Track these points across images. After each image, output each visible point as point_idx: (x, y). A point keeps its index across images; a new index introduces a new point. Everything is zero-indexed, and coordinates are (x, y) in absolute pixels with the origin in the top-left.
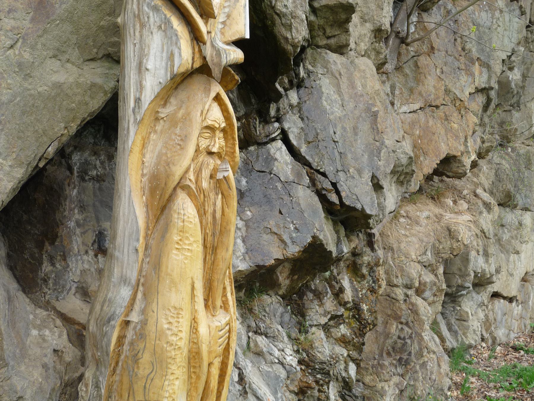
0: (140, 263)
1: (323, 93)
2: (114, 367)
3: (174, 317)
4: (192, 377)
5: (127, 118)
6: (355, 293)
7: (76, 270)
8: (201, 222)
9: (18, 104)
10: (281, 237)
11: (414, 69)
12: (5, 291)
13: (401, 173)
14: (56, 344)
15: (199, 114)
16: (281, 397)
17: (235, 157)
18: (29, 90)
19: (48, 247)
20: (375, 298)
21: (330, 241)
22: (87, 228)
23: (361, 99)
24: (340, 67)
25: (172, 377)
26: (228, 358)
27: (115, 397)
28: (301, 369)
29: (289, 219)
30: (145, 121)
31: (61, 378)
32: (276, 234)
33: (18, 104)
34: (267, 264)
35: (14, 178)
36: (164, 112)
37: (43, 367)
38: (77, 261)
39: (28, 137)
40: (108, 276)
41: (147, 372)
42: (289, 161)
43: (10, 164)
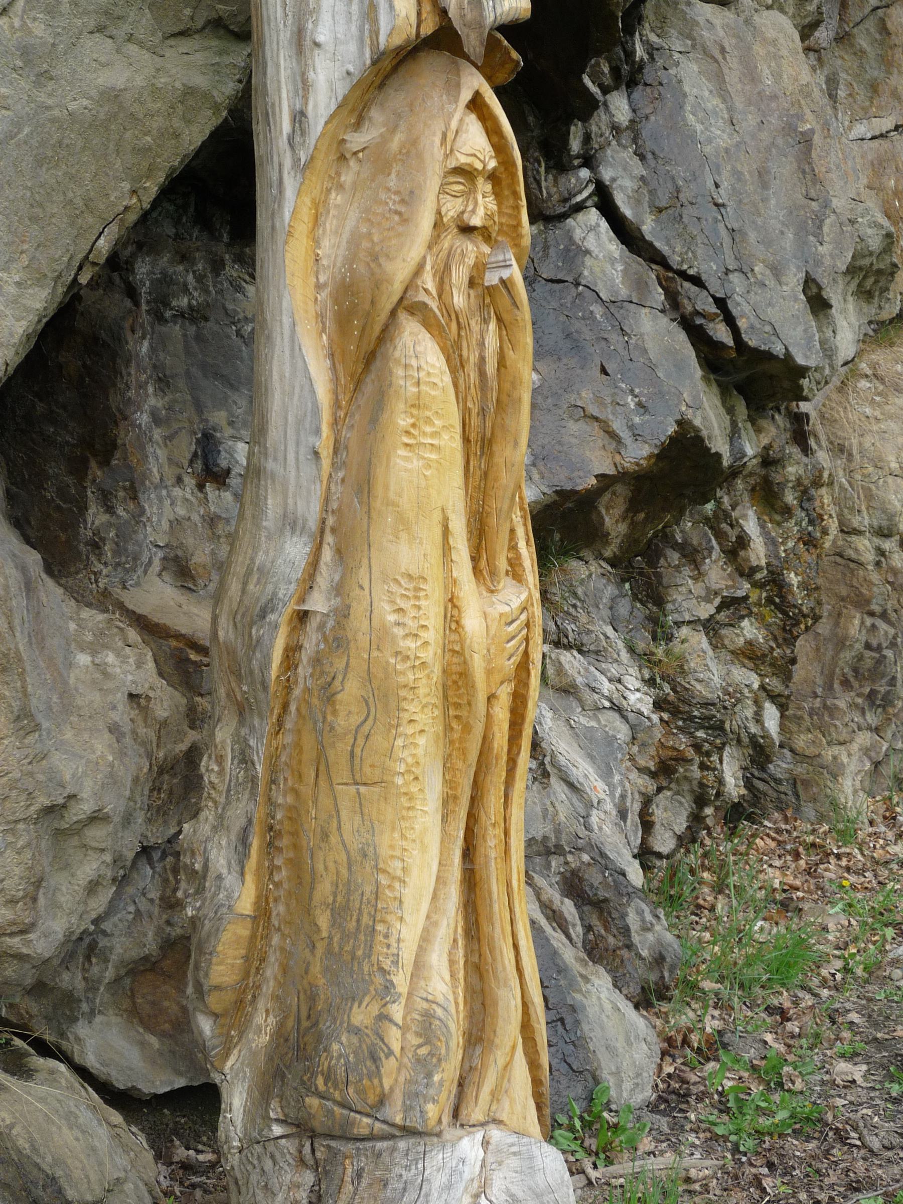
0: (325, 482)
1: (685, 95)
2: (280, 716)
3: (407, 597)
4: (452, 729)
5: (275, 158)
6: (771, 548)
7: (159, 521)
8: (456, 385)
9: (25, 142)
10: (609, 426)
11: (878, 36)
12: (17, 568)
13: (867, 272)
14: (133, 682)
15: (437, 140)
16: (621, 782)
17: (520, 236)
18: (48, 108)
19: (96, 471)
20: (814, 557)
21: (717, 432)
22: (175, 426)
23: (773, 105)
24: (721, 33)
25: (410, 730)
26: (527, 685)
27: (286, 779)
28: (661, 719)
29: (623, 386)
30: (318, 163)
31: (149, 755)
32: (596, 419)
33: (25, 142)
34: (579, 488)
35: (28, 310)
36: (357, 140)
37: (110, 731)
38: (160, 499)
40: (253, 517)
41: (356, 720)
42: (617, 255)
43: (17, 278)
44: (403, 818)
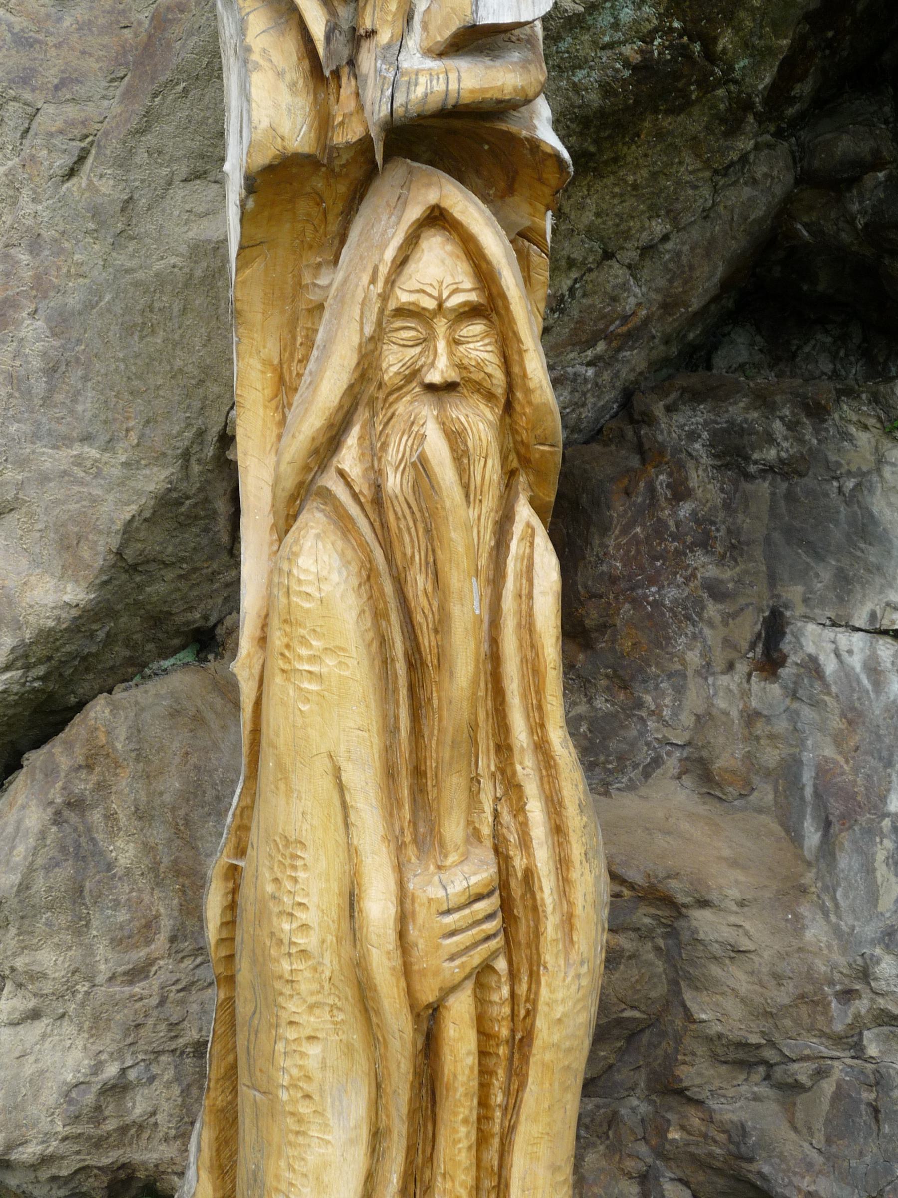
9: (109, 311)
15: (366, 278)
22: (742, 601)
25: (291, 1034)
33: (109, 311)
35: (138, 493)
39: (158, 388)
43: (123, 459)
44: (290, 1143)
